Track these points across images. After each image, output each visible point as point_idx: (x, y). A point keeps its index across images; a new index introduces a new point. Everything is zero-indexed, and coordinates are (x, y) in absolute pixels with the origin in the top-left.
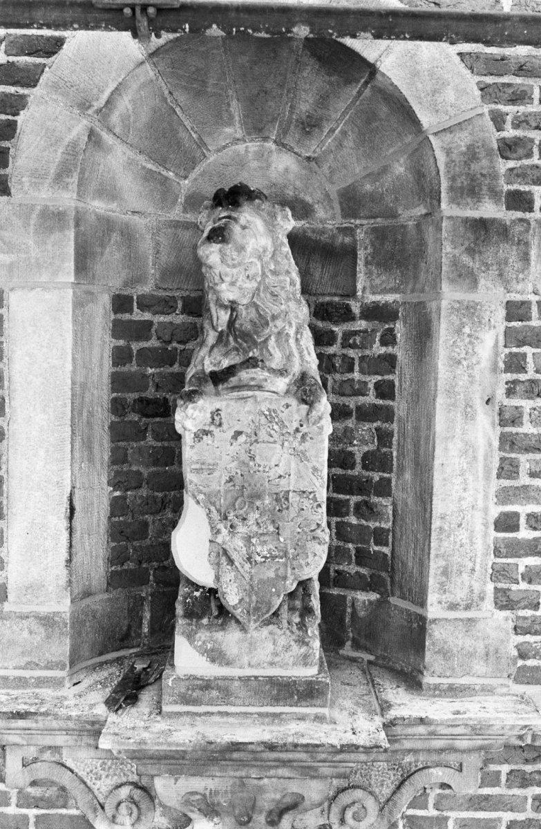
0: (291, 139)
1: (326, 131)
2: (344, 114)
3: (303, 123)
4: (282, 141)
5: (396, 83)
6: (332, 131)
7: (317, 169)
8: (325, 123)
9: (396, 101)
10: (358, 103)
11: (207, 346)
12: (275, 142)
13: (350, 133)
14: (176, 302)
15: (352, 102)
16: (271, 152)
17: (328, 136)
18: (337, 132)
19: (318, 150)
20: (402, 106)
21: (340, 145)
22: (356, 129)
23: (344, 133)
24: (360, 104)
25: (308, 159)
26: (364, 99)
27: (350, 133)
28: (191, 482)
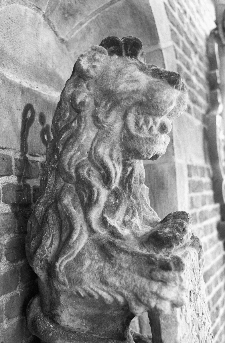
0: (55, 18)
1: (78, 23)
2: (94, 14)
3: (64, 8)
4: (49, 17)
5: (151, 5)
6: (81, 24)
7: (67, 52)
8: (78, 16)
9: (143, 17)
10: (107, 9)
11: (99, 207)
12: (44, 16)
13: (93, 30)
14: (194, 182)
15: (102, 7)
16: (40, 23)
17: (77, 28)
18: (84, 26)
19: (69, 36)
20: (148, 23)
21: (84, 38)
22: (98, 29)
23: (88, 29)
24: (109, 11)
25: (63, 40)
26: (113, 8)
27: (93, 30)
28: (162, 323)
